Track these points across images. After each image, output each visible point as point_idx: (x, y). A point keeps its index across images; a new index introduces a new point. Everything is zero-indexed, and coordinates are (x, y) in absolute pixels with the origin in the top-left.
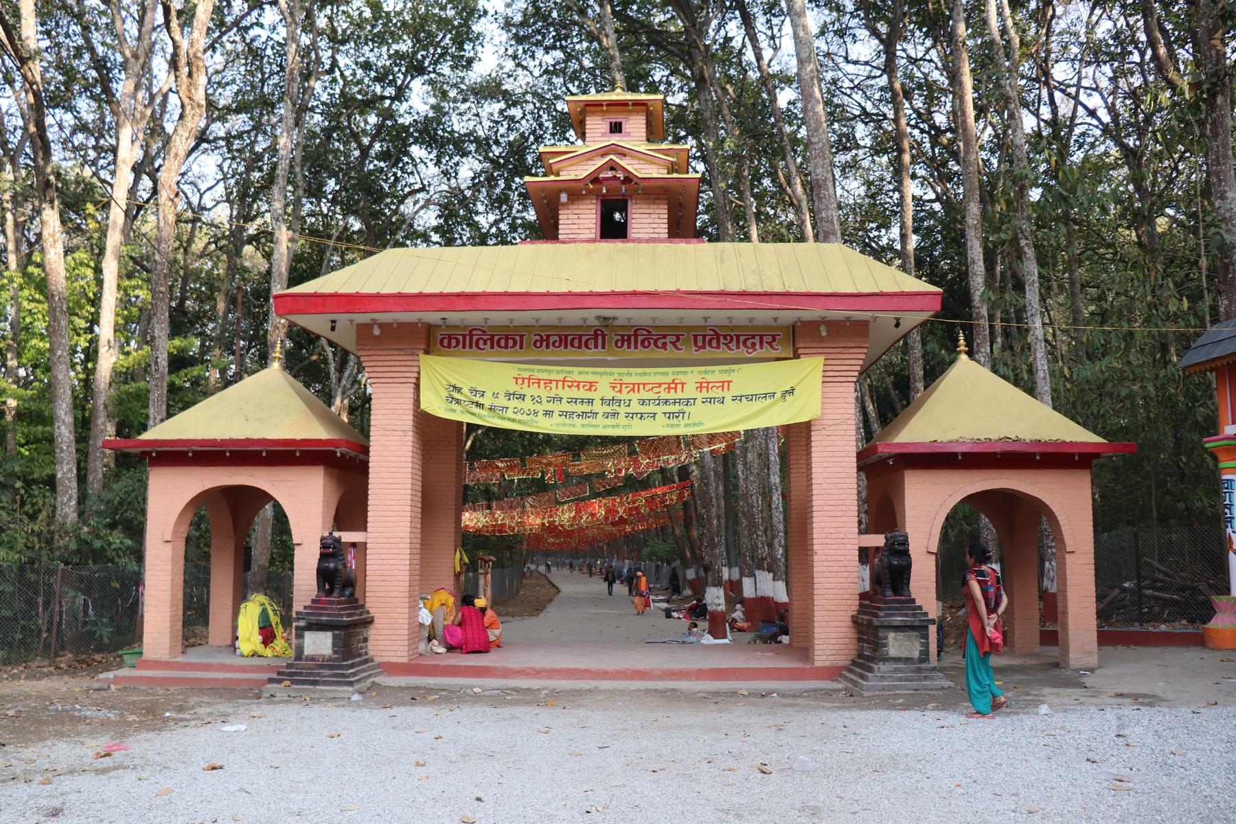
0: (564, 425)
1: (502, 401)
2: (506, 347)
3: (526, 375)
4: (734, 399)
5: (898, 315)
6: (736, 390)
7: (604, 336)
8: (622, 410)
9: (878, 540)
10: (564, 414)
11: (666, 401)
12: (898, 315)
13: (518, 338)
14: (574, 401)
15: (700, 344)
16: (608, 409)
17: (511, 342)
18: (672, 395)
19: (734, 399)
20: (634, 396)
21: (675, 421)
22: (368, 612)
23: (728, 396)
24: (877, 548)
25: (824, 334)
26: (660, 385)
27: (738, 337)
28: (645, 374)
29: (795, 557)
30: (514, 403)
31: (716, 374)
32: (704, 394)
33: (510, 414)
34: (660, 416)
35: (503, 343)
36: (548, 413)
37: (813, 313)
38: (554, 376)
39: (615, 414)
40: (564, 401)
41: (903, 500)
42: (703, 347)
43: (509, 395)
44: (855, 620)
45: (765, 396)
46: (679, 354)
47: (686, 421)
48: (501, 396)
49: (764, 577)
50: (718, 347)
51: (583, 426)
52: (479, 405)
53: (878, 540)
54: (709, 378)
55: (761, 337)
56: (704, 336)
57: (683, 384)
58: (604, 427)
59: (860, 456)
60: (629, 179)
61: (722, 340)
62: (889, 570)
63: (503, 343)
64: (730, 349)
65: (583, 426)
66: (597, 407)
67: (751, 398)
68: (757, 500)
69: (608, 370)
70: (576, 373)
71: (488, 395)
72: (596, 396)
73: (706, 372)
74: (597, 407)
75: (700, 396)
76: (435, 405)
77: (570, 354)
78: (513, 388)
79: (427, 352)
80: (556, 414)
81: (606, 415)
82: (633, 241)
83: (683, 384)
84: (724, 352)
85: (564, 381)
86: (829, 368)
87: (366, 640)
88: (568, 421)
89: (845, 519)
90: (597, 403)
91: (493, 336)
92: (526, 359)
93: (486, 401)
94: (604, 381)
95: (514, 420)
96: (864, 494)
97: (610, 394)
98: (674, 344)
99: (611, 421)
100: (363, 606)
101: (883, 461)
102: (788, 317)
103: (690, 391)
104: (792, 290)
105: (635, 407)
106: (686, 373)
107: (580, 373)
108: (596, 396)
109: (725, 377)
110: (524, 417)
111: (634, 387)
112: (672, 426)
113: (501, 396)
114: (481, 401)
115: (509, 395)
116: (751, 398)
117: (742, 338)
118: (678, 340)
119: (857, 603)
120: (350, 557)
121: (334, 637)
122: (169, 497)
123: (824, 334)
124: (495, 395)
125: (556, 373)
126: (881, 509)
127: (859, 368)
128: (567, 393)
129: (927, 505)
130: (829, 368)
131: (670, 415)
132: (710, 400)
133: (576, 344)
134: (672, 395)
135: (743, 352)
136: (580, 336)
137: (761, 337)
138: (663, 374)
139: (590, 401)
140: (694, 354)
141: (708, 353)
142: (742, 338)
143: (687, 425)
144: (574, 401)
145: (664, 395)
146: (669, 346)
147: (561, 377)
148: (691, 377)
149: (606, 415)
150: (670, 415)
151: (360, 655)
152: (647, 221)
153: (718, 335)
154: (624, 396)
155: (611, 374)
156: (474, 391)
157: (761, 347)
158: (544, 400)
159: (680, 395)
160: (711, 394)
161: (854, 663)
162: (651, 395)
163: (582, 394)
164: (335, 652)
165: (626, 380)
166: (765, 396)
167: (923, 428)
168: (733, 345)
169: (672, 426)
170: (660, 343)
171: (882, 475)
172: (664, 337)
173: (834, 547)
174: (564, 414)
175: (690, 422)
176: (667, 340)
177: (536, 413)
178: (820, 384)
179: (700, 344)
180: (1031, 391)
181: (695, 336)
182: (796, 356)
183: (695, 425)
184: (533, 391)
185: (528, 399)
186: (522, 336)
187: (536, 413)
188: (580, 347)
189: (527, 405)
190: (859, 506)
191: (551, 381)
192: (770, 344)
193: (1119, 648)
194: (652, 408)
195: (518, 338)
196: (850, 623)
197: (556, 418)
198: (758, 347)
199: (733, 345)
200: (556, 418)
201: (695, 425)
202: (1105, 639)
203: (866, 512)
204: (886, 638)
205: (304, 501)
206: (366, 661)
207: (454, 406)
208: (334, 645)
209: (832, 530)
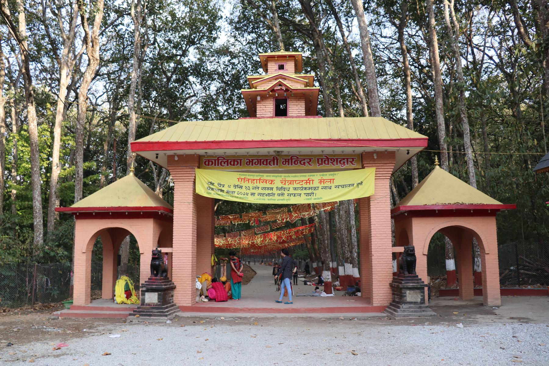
0: (260, 199)
2: (234, 165)
3: (243, 177)
6: (336, 183)
8: (286, 192)
9: (401, 249)
10: (260, 194)
11: (306, 188)
13: (239, 161)
15: (320, 163)
16: (280, 192)
17: (236, 163)
20: (291, 186)
21: (310, 197)
25: (375, 157)
26: (303, 181)
27: (337, 159)
31: (327, 176)
32: (322, 185)
35: (232, 163)
36: (253, 194)
38: (255, 178)
41: (412, 231)
42: (322, 164)
43: (235, 186)
45: (350, 185)
48: (232, 187)
50: (328, 164)
51: (269, 200)
52: (222, 191)
53: (401, 249)
54: (325, 178)
56: (322, 159)
57: (313, 180)
61: (330, 161)
62: (406, 263)
63: (232, 163)
64: (310, 164)
65: (269, 200)
66: (275, 191)
67: (343, 186)
70: (265, 176)
71: (226, 186)
74: (275, 191)
75: (321, 186)
76: (202, 191)
77: (262, 168)
78: (237, 183)
79: (199, 167)
80: (256, 195)
81: (279, 195)
82: (290, 117)
83: (313, 180)
85: (260, 180)
86: (378, 173)
88: (262, 197)
89: (386, 240)
90: (275, 189)
91: (228, 160)
92: (240, 170)
93: (225, 189)
94: (278, 179)
95: (237, 197)
97: (280, 185)
98: (308, 163)
99: (281, 197)
101: (402, 214)
103: (316, 184)
104: (361, 138)
105: (292, 191)
107: (267, 176)
109: (331, 177)
110: (242, 196)
111: (291, 182)
112: (308, 199)
113: (232, 187)
115: (235, 186)
116: (343, 186)
117: (339, 160)
118: (310, 161)
122: (84, 233)
123: (375, 157)
124: (229, 186)
125: (256, 176)
126: (401, 235)
128: (261, 185)
129: (423, 233)
131: (307, 194)
132: (325, 188)
133: (265, 163)
135: (339, 166)
136: (267, 160)
139: (272, 189)
142: (339, 160)
143: (315, 199)
145: (305, 186)
146: (307, 164)
147: (258, 178)
148: (316, 177)
150: (307, 194)
153: (328, 159)
156: (220, 184)
158: (251, 188)
159: (311, 185)
160: (326, 185)
165: (288, 179)
166: (350, 185)
168: (335, 163)
170: (302, 162)
171: (402, 220)
172: (304, 160)
174: (260, 194)
175: (316, 197)
176: (306, 161)
177: (247, 194)
179: (320, 163)
180: (466, 180)
181: (318, 159)
182: (363, 167)
186: (241, 160)
187: (247, 194)
189: (244, 190)
191: (254, 180)
192: (351, 162)
194: (299, 192)
195: (239, 161)
198: (346, 164)
199: (335, 163)
202: (503, 292)
204: (405, 293)
205: (145, 234)
207: (210, 191)
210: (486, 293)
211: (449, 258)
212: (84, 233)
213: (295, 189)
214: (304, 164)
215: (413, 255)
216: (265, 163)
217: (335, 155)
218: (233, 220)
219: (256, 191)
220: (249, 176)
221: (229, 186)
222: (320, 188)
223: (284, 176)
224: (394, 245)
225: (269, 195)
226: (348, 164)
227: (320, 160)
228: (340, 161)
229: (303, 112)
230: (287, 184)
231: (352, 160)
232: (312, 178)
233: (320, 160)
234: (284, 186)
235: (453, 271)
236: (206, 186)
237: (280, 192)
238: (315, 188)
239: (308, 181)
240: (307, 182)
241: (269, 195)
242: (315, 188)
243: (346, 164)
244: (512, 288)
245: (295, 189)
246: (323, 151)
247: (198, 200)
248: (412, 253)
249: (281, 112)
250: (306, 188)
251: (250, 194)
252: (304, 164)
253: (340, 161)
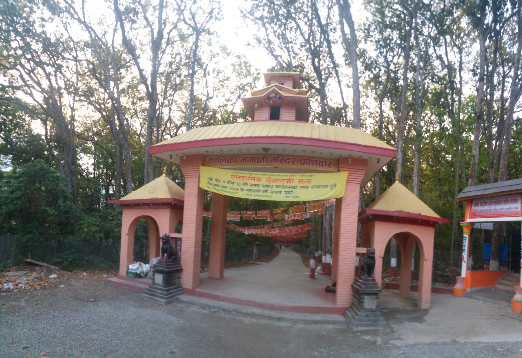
0: (248, 195)
1: (226, 184)
2: (231, 162)
3: (235, 174)
4: (313, 187)
5: (378, 157)
6: (313, 183)
7: (267, 158)
8: (270, 189)
9: (363, 250)
10: (248, 190)
11: (286, 187)
12: (378, 157)
13: (235, 159)
14: (252, 185)
15: (302, 163)
16: (264, 189)
17: (232, 161)
18: (289, 184)
19: (313, 187)
20: (274, 184)
21: (288, 195)
22: (181, 266)
23: (310, 185)
24: (363, 254)
25: (350, 162)
26: (284, 180)
27: (317, 161)
28: (279, 175)
29: (335, 253)
30: (230, 185)
31: (306, 176)
32: (301, 184)
33: (228, 190)
34: (283, 193)
35: (229, 161)
36: (242, 190)
37: (345, 153)
38: (246, 175)
39: (267, 191)
40: (249, 185)
41: (373, 234)
42: (304, 164)
43: (229, 182)
44: (352, 286)
45: (324, 186)
46: (295, 166)
47: (293, 195)
48: (226, 182)
49: (328, 256)
50: (309, 165)
51: (255, 195)
52: (218, 186)
53: (363, 250)
54: (304, 178)
55: (326, 162)
56: (304, 160)
57: (293, 180)
58: (263, 196)
59: (360, 214)
60: (281, 97)
61: (311, 162)
62: (365, 267)
63: (229, 161)
64: (293, 164)
65: (255, 195)
66: (261, 188)
67: (318, 187)
68: (328, 230)
69: (266, 173)
70: (254, 174)
71: (222, 182)
72: (260, 183)
73: (303, 176)
74: (261, 188)
75: (299, 185)
76: (204, 186)
77: (253, 165)
78: (230, 179)
79: (203, 165)
80: (245, 190)
81: (264, 191)
82: (283, 121)
83: (293, 180)
84: (310, 167)
85: (249, 177)
86: (350, 177)
87: (179, 278)
88: (249, 193)
89: (352, 240)
90: (261, 186)
91: (226, 159)
92: (232, 167)
93: (221, 184)
94: (264, 178)
95: (229, 192)
96: (360, 231)
97: (265, 183)
98: (292, 162)
99: (265, 194)
100: (179, 264)
101: (368, 217)
102: (337, 153)
103: (296, 183)
104: (339, 140)
105: (274, 189)
106: (305, 176)
107: (256, 174)
108: (260, 183)
109: (309, 178)
110: (233, 191)
111: (275, 180)
112: (287, 197)
113: (226, 182)
114: (219, 184)
115: (229, 182)
116: (318, 187)
117: (318, 162)
118: (294, 161)
119: (353, 278)
120: (262, 226)
121: (164, 277)
122: (128, 219)
123: (350, 162)
124: (224, 182)
125: (246, 174)
126: (365, 238)
127: (362, 178)
128: (250, 182)
129: (383, 236)
130: (350, 177)
131: (287, 192)
132: (303, 187)
133: (256, 161)
134: (289, 184)
135: (318, 168)
136: (258, 158)
137: (326, 162)
138: (286, 176)
139: (258, 185)
140: (300, 167)
141: (305, 167)
142: (318, 162)
143: (293, 197)
144: (252, 185)
145: (286, 184)
146: (291, 163)
147: (248, 176)
148: (297, 177)
149: (264, 191)
150: (287, 192)
151: (175, 285)
152: (286, 114)
153: (309, 160)
154: (270, 184)
155: (267, 175)
156: (217, 180)
157: (325, 166)
158: (241, 184)
159: (291, 185)
160: (304, 185)
161: (351, 307)
162: (281, 184)
163: (256, 182)
164: (163, 283)
165: (272, 177)
166: (324, 186)
167: (382, 206)
168: (314, 164)
169: (287, 197)
170: (287, 162)
171: (367, 221)
172: (289, 159)
173: (347, 252)
174: (248, 190)
175: (295, 196)
176: (290, 160)
177: (238, 189)
178: (345, 183)
179: (302, 163)
180: (412, 191)
181: (301, 160)
182: (339, 171)
183: (296, 197)
184: (237, 181)
185: (235, 184)
186: (236, 158)
187: (238, 189)
188: (258, 162)
189: (235, 186)
190: (357, 235)
191: (244, 177)
192: (329, 166)
193: (411, 212)
194: (280, 189)
195: (235, 159)
196: (350, 287)
197: (245, 192)
198: (324, 166)
199: (314, 164)
200: (245, 192)
201: (296, 197)
202: (434, 290)
203: (360, 237)
204: (364, 299)
205: (164, 221)
206: (178, 287)
207: (209, 186)
208: (163, 280)
209: (346, 245)
210: (421, 290)
211: (394, 257)
212: (128, 219)
213: (277, 187)
214: (289, 163)
215: (373, 258)
216: (256, 161)
217: (315, 157)
218: (265, 214)
219: (245, 187)
220: (241, 173)
221: (224, 182)
222: (298, 188)
223: (270, 175)
224: (358, 246)
225: (255, 191)
226: (325, 166)
227: (303, 161)
228: (319, 163)
229: (293, 118)
230: (271, 182)
231: (329, 163)
232: (293, 178)
233: (303, 161)
234: (269, 184)
235: (396, 267)
236: (207, 181)
237: (264, 189)
238: (294, 187)
239: (289, 181)
240: (288, 182)
241: (255, 191)
242: (294, 187)
243: (324, 166)
244: (448, 288)
245: (277, 187)
246: (304, 151)
247: (202, 193)
248: (372, 255)
249: (275, 116)
250: (286, 187)
251: (240, 189)
252: (289, 163)
253: (319, 163)
